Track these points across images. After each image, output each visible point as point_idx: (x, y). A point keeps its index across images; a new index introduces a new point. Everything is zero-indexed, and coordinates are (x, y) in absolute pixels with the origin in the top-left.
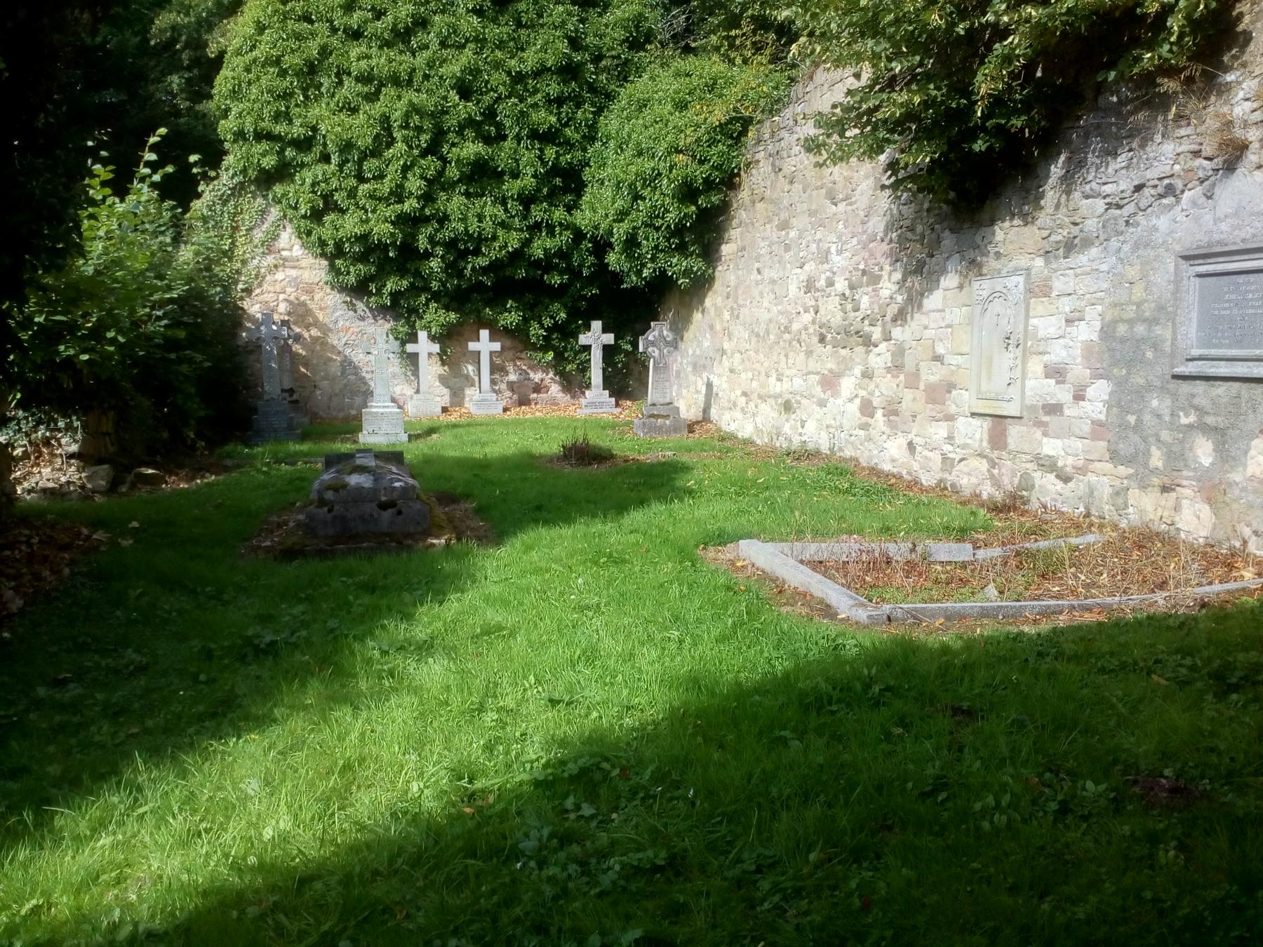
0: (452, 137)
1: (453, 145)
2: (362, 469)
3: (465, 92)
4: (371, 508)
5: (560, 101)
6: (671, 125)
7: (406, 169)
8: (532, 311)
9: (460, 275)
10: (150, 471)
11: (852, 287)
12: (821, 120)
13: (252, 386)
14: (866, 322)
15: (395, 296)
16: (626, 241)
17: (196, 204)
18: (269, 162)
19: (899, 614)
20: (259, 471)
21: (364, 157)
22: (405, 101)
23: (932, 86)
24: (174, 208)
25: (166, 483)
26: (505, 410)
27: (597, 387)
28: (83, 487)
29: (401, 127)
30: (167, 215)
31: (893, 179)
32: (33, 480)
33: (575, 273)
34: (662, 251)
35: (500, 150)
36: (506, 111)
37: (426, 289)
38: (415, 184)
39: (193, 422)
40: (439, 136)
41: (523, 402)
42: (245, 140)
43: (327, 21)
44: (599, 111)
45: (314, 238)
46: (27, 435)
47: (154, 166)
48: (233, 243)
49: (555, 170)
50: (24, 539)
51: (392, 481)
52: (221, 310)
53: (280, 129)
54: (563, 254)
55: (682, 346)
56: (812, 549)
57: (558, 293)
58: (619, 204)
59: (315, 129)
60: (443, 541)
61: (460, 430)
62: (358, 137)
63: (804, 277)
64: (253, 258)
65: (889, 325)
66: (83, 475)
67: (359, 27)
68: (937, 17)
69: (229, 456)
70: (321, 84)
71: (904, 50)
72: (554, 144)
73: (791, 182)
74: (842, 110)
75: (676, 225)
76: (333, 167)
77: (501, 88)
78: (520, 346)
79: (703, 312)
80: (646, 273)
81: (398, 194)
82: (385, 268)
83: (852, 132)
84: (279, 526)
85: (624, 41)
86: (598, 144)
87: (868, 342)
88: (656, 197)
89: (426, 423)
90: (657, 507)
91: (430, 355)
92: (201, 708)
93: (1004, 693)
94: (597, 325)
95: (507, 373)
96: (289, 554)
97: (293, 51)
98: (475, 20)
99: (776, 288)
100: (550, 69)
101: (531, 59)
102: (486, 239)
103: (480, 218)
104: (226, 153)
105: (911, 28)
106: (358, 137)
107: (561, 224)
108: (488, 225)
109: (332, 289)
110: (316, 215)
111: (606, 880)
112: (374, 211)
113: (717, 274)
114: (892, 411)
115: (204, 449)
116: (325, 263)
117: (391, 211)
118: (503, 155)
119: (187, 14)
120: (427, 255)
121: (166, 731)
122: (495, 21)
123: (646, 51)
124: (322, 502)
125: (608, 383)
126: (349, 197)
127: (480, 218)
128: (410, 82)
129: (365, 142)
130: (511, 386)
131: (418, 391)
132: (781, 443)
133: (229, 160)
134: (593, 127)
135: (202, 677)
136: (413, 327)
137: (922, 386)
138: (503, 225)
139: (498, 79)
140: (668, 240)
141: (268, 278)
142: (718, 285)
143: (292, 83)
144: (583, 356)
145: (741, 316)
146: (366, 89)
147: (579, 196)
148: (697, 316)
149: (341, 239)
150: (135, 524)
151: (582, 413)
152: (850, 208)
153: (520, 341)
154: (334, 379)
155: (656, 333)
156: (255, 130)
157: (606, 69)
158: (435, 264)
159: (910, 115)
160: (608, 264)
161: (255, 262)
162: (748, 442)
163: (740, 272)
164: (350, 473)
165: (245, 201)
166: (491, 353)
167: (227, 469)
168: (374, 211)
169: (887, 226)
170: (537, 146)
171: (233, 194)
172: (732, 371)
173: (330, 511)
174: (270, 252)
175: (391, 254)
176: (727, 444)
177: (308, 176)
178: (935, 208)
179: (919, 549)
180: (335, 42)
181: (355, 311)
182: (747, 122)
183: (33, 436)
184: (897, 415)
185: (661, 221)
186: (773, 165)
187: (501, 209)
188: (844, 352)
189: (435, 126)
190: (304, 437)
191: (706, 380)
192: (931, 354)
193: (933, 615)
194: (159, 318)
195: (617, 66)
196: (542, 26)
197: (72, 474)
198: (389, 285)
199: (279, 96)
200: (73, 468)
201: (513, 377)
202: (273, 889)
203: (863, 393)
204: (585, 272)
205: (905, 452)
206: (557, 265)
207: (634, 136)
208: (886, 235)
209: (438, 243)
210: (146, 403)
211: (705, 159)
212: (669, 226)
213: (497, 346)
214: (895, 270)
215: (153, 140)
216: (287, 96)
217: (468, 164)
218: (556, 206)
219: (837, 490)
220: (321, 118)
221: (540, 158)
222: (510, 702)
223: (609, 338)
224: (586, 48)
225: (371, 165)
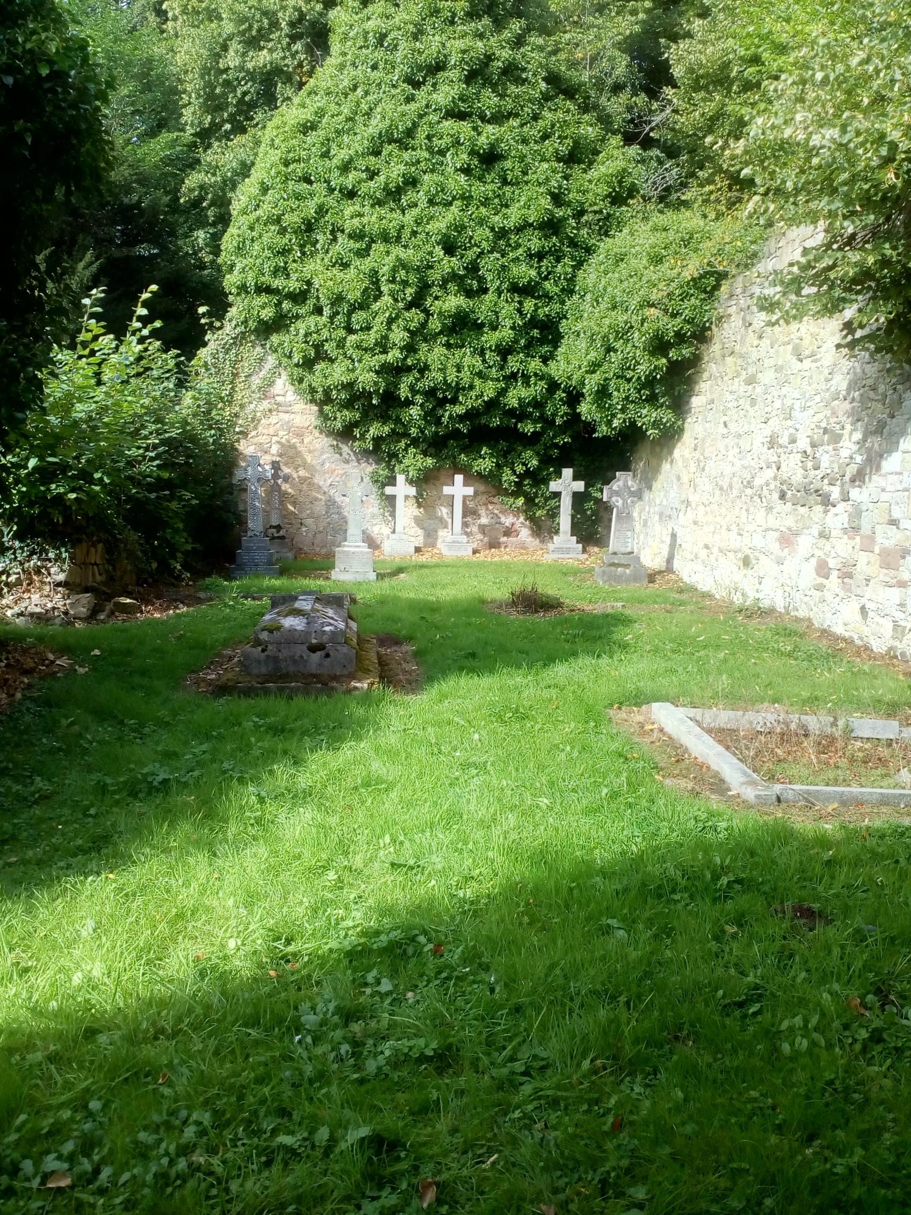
0: (435, 290)
1: (437, 298)
2: (298, 613)
3: (450, 249)
4: (301, 650)
5: (540, 256)
6: (645, 279)
7: (391, 321)
8: (505, 458)
9: (438, 422)
10: (128, 601)
11: (814, 445)
12: (777, 277)
13: (241, 521)
14: (826, 481)
15: (377, 441)
16: (598, 392)
17: (203, 353)
18: (267, 314)
19: (790, 795)
20: (226, 605)
21: (353, 309)
22: (392, 257)
23: (887, 246)
24: (178, 356)
25: (142, 612)
26: (475, 552)
27: (565, 533)
28: (66, 613)
29: (388, 280)
30: (172, 363)
31: (850, 338)
32: (24, 605)
33: (549, 423)
34: (632, 402)
35: (481, 302)
36: (489, 264)
37: (406, 435)
38: (398, 336)
39: (179, 555)
40: (424, 288)
41: (493, 544)
42: (247, 293)
43: (325, 181)
44: (579, 265)
45: (305, 385)
46: (21, 564)
47: (145, 321)
49: (533, 322)
51: (323, 625)
52: (215, 451)
53: (277, 283)
54: (538, 404)
55: (647, 495)
56: (724, 717)
57: (532, 440)
58: (593, 356)
59: (309, 283)
60: (366, 685)
61: (427, 571)
62: (348, 291)
63: (768, 433)
64: (250, 403)
65: (847, 486)
66: (68, 602)
67: (354, 186)
68: (893, 176)
70: (317, 241)
71: (858, 208)
72: (533, 297)
73: (760, 337)
74: (799, 269)
75: (647, 377)
76: (324, 319)
77: (484, 244)
78: (494, 492)
79: (672, 462)
80: (616, 423)
81: (383, 346)
82: (369, 414)
83: (808, 290)
85: (607, 196)
86: (576, 297)
87: (827, 502)
88: (628, 350)
89: (398, 562)
90: (585, 661)
91: (407, 497)
92: (79, 842)
93: (864, 895)
94: (568, 472)
95: (479, 516)
96: (222, 690)
97: (292, 210)
98: (462, 178)
99: (741, 442)
100: (531, 225)
101: (514, 216)
102: (464, 389)
103: (459, 368)
104: (231, 305)
105: (866, 187)
106: (348, 291)
107: (536, 375)
108: (466, 376)
109: (321, 433)
110: (308, 364)
111: (371, 1066)
112: (360, 361)
113: (686, 425)
114: (846, 574)
115: (190, 579)
116: (315, 408)
117: (376, 361)
118: (483, 308)
119: (214, 175)
120: (408, 403)
121: (39, 863)
122: (481, 179)
123: (628, 205)
124: (258, 642)
125: (576, 529)
126: (338, 347)
127: (459, 368)
128: (398, 238)
129: (354, 295)
130: (483, 529)
131: (394, 532)
132: (737, 600)
133: (233, 312)
134: (571, 280)
136: (393, 471)
137: (877, 550)
138: (480, 375)
139: (482, 235)
140: (639, 392)
141: (263, 421)
142: (687, 437)
143: (290, 241)
144: (552, 503)
145: (707, 468)
146: (358, 245)
147: (556, 347)
148: (666, 467)
149: (329, 387)
150: (97, 652)
151: (549, 558)
152: (815, 365)
153: (494, 486)
154: (317, 518)
155: (621, 483)
156: (256, 284)
157: (588, 224)
158: (415, 412)
159: (864, 275)
160: (579, 415)
161: (252, 406)
162: (708, 596)
163: (708, 425)
164: (286, 616)
165: (245, 350)
166: (465, 498)
167: (199, 601)
168: (360, 361)
169: (850, 384)
170: (517, 299)
171: (234, 343)
172: (695, 523)
173: (263, 651)
174: (266, 397)
175: (374, 402)
176: (684, 597)
177: (301, 327)
178: (896, 368)
179: (841, 723)
180: (331, 201)
181: (341, 454)
182: (722, 276)
183: (26, 565)
184: (851, 578)
185: (632, 373)
186: (744, 319)
187: (479, 359)
188: (802, 510)
189: (421, 280)
190: (282, 572)
191: (670, 531)
192: (887, 517)
193: (828, 798)
194: (152, 459)
195: (599, 220)
196: (527, 183)
197: (58, 601)
198: (372, 431)
199: (278, 252)
200: (59, 596)
201: (484, 520)
202: (60, 1036)
203: (818, 553)
204: (558, 421)
205: (858, 617)
206: (531, 414)
207: (609, 289)
208: (848, 394)
209: (418, 392)
210: (134, 536)
211: (677, 313)
212: (639, 378)
213: (470, 491)
214: (855, 430)
215: (145, 296)
216: (285, 252)
217: (450, 316)
218: (533, 357)
219: (780, 653)
220: (315, 273)
221: (519, 311)
222: (358, 861)
223: (580, 486)
224: (569, 204)
225: (359, 317)
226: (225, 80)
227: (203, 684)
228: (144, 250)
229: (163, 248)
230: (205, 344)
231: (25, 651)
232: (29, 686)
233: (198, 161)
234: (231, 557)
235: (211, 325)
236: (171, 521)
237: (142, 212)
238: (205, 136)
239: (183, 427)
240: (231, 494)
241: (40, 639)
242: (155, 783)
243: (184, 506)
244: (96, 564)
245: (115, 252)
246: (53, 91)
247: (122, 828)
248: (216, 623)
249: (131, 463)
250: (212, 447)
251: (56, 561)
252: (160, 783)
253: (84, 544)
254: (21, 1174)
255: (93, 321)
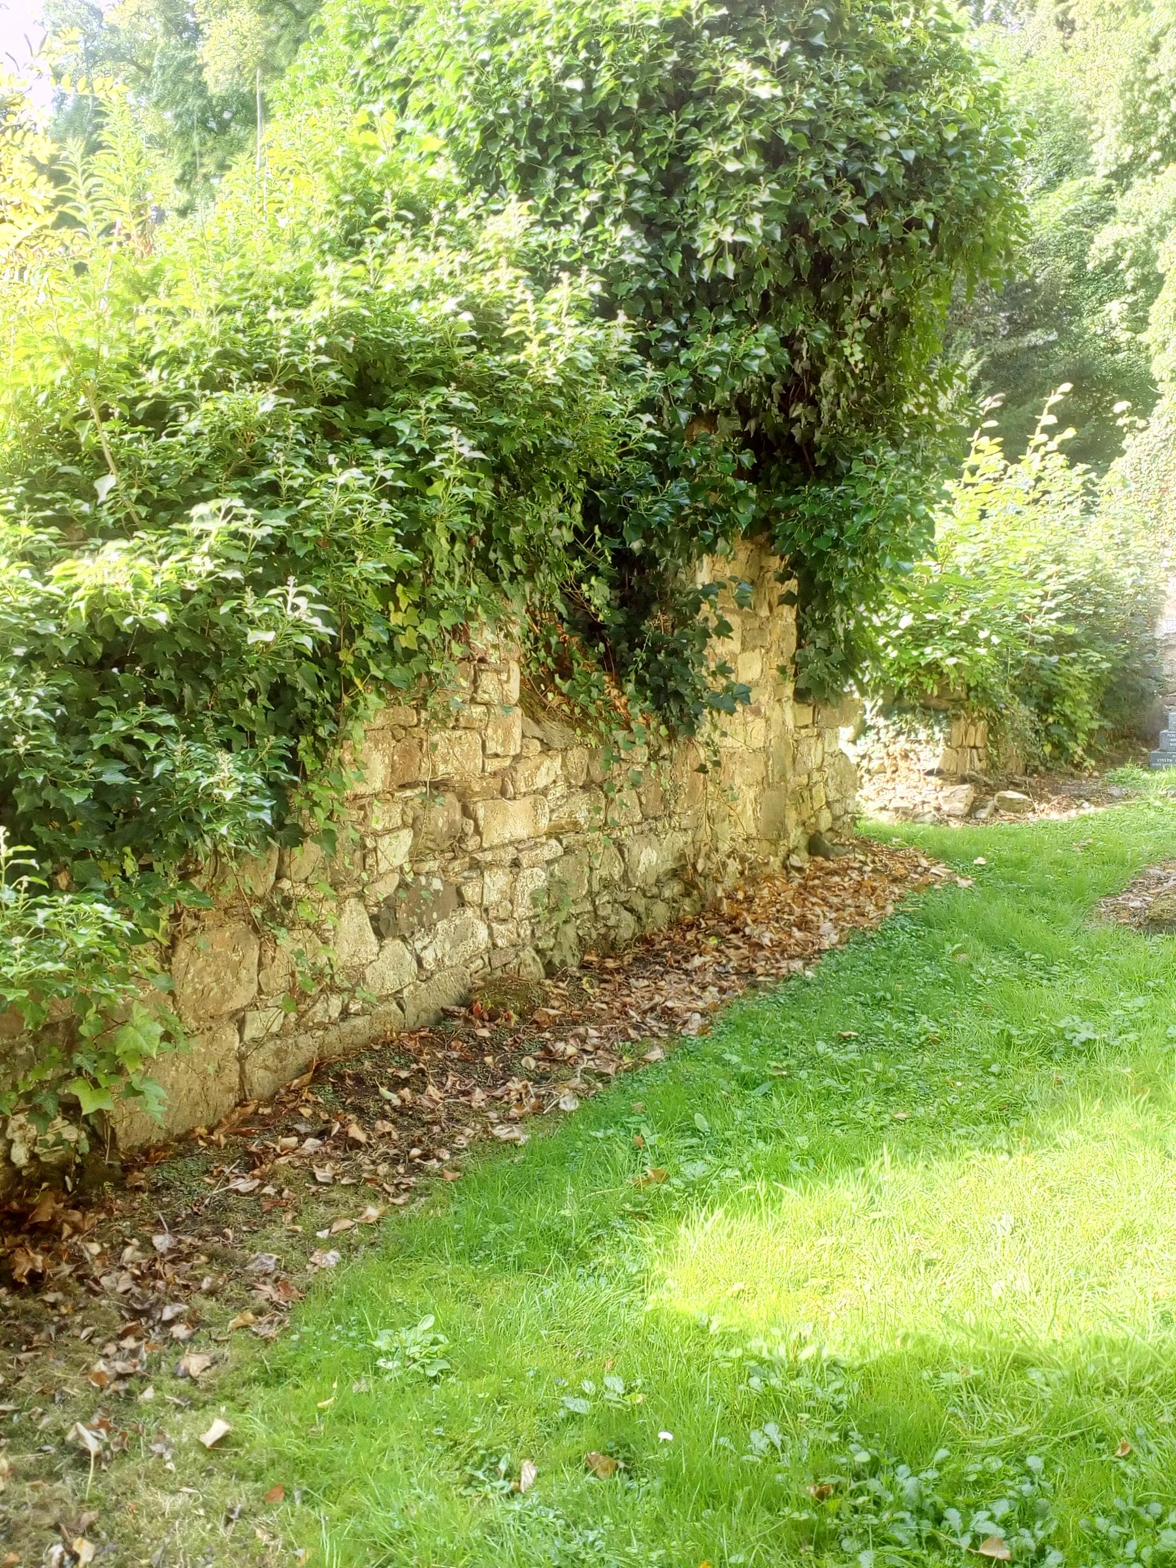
24: (1086, 472)
30: (1077, 484)
32: (888, 797)
39: (1081, 735)
46: (886, 746)
47: (1050, 431)
48: (1160, 509)
50: (857, 865)
69: (1121, 781)
84: (1160, 881)
92: (981, 1106)
115: (1094, 769)
135: (995, 1068)
150: (981, 860)
167: (1111, 799)
183: (891, 749)
194: (1050, 611)
202: (980, 1359)
215: (1054, 399)
226: (1155, 93)
227: (1124, 914)
228: (1036, 337)
229: (1063, 332)
230: (1122, 453)
231: (892, 854)
232: (902, 898)
233: (1113, 210)
234: (1150, 739)
235: (1131, 426)
236: (1072, 691)
237: (1036, 290)
238: (1122, 175)
239: (1092, 566)
240: (1154, 653)
241: (910, 840)
242: (1076, 1043)
243: (1091, 671)
244: (975, 747)
245: (1003, 347)
246: (960, 157)
247: (1035, 1097)
248: (1136, 830)
249: (1022, 618)
250: (1131, 591)
251: (928, 742)
252: (1083, 1043)
253: (962, 721)
254: (944, 1523)
255: (986, 439)
